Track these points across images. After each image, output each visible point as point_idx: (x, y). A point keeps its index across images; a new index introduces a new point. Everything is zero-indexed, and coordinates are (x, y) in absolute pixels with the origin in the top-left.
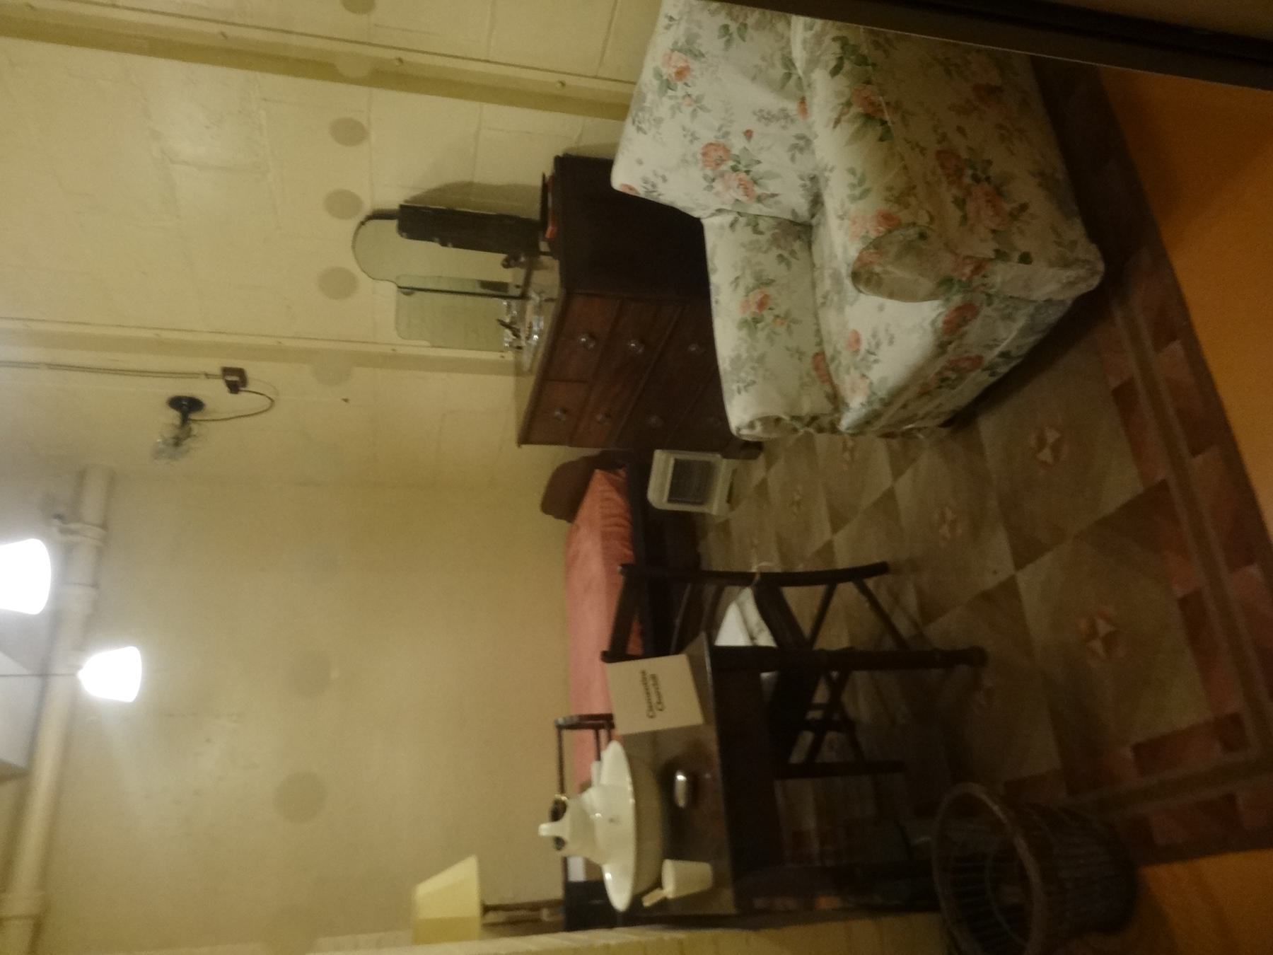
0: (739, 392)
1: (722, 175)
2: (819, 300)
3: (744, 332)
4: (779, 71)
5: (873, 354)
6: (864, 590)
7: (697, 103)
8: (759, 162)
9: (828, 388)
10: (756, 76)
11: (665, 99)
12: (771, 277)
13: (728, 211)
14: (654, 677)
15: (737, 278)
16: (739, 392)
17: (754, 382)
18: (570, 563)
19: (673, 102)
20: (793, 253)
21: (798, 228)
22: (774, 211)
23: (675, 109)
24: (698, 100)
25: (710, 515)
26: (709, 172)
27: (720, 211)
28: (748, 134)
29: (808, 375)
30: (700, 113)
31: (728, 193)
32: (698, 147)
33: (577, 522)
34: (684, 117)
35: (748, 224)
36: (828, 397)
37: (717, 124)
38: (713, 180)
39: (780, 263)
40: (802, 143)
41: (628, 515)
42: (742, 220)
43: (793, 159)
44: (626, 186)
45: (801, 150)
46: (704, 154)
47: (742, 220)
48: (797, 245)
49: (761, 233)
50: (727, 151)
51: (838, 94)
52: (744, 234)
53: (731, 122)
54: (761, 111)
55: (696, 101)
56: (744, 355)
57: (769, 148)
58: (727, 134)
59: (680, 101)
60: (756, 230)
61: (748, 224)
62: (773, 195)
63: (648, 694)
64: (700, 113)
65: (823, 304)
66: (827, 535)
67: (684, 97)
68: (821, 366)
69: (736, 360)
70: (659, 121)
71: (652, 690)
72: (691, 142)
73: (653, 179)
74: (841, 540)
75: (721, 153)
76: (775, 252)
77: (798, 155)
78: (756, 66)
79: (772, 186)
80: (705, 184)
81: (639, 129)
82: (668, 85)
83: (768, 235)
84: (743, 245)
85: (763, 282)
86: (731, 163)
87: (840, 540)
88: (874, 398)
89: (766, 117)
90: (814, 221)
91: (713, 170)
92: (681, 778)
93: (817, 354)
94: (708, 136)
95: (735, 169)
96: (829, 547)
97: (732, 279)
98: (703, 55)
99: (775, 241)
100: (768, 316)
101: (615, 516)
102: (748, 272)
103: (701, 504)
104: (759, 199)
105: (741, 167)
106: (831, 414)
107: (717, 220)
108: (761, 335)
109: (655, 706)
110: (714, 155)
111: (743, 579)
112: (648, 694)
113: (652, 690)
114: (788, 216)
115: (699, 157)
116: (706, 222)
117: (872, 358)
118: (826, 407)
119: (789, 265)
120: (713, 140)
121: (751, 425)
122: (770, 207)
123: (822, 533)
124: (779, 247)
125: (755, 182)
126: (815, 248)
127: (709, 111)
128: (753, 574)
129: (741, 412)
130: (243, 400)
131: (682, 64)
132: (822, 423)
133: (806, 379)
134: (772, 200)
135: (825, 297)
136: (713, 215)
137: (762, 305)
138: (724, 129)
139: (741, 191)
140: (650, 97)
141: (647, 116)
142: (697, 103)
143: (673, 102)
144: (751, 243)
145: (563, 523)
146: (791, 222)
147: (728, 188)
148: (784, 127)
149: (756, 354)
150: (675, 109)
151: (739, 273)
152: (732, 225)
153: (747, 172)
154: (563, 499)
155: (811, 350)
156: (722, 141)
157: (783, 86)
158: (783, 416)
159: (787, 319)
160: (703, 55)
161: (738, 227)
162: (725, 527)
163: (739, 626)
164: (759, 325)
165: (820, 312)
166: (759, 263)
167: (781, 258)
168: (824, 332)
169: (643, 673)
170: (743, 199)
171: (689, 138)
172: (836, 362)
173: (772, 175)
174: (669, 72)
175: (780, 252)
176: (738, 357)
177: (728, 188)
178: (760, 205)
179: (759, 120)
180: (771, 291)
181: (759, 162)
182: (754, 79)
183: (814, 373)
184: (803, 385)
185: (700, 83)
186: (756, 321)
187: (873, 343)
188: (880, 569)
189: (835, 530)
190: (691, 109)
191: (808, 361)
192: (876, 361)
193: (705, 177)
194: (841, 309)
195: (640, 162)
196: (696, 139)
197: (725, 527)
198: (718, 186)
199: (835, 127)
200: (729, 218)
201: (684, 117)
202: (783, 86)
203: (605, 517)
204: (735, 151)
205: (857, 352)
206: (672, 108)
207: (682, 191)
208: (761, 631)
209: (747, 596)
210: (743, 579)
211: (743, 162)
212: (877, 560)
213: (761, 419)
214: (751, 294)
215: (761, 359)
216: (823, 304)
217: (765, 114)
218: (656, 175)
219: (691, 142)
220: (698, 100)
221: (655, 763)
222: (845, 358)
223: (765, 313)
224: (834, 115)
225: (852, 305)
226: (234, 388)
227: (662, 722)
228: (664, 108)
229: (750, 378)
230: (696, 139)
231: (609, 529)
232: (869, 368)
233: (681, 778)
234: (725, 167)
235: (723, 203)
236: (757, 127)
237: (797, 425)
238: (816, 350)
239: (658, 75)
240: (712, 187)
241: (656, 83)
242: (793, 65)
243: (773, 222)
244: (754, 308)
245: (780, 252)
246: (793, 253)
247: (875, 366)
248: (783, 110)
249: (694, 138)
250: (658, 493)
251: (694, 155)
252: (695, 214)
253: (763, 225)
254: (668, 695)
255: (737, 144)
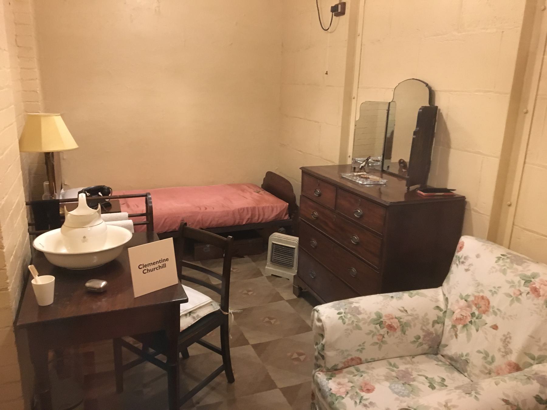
0: (339, 314)
1: (469, 306)
2: (392, 361)
3: (374, 316)
4: (536, 354)
5: (360, 402)
6: (217, 373)
7: (516, 298)
8: (477, 330)
9: (341, 366)
10: (533, 338)
11: (518, 278)
12: (407, 333)
13: (447, 306)
14: (165, 266)
15: (406, 311)
16: (339, 314)
17: (344, 323)
18: (238, 186)
19: (516, 283)
20: (421, 344)
21: (436, 347)
22: (446, 335)
23: (512, 284)
24: (518, 300)
25: (266, 265)
26: (471, 299)
27: (447, 299)
28: (495, 327)
29: (348, 355)
30: (377, 346)
31: (457, 307)
32: (487, 294)
33: (262, 192)
34: (506, 289)
35: (438, 317)
36: (335, 365)
37: (502, 309)
38: (466, 300)
39: (415, 337)
40: (489, 359)
41: (264, 221)
42: (441, 314)
43: (479, 352)
44: (463, 245)
45: (485, 358)
46: (483, 298)
47: (441, 314)
48: (426, 347)
49: (433, 326)
50: (485, 312)
51: (524, 402)
52: (433, 315)
53: (503, 318)
54: (510, 338)
55: (517, 297)
56: (360, 317)
57: (486, 338)
58: (495, 313)
59: (517, 288)
60: (435, 322)
61: (438, 317)
62: (456, 336)
63: (154, 264)
64: (377, 346)
65: (390, 364)
66: (252, 342)
67: (520, 291)
68: (354, 362)
69: (357, 311)
70: (504, 272)
71: (156, 266)
72: (491, 291)
73: (467, 263)
74: (249, 351)
75: (483, 308)
76: (421, 334)
77: (482, 355)
78: (540, 339)
79: (462, 336)
80: (464, 295)
81: (499, 258)
82: (528, 281)
83: (432, 330)
84: (426, 314)
85: (404, 327)
86: (477, 313)
87: (249, 351)
88: (334, 398)
89: (506, 340)
90: (439, 356)
91: (472, 301)
92: (103, 284)
93: (360, 359)
94: (494, 302)
95: (473, 315)
96: (245, 342)
97: (406, 309)
98: (404, 334)
99: (428, 334)
100: (383, 331)
101: (264, 215)
102: (410, 318)
103: (271, 261)
104: (454, 327)
105: (475, 318)
106: (325, 366)
107: (441, 298)
108: (372, 327)
109: (145, 268)
110: (482, 303)
111: (225, 306)
112: (154, 264)
113: (156, 266)
114: (443, 342)
115: (481, 294)
116: (439, 290)
117: (358, 401)
118: (329, 365)
119: (414, 342)
120: (491, 304)
121: (319, 320)
122: (450, 332)
123: (253, 338)
124: (425, 336)
125: (465, 326)
126: (424, 357)
127: (511, 305)
128: (228, 311)
129: (327, 312)
130: (327, 14)
131: (542, 292)
132: (319, 361)
133: (346, 354)
134: (454, 334)
135: (395, 366)
136: (444, 295)
137: (390, 327)
138: (498, 313)
139: (459, 316)
140: (520, 268)
141: (507, 265)
142: (516, 298)
143: (516, 283)
144: (428, 319)
145: (262, 182)
146: (440, 343)
147: (461, 309)
148: (499, 350)
149: (361, 324)
150: (512, 284)
151: (409, 312)
152: (438, 307)
153: (471, 322)
154: (274, 185)
155: (363, 357)
156: (491, 310)
157: (526, 354)
158: (324, 340)
159: (381, 342)
160: (404, 334)
161: (437, 311)
162: (259, 274)
163: (197, 303)
164: (378, 326)
165: (384, 362)
166: (415, 326)
167: (418, 338)
168: (374, 364)
169: (167, 260)
170: (454, 317)
171: (494, 290)
172: (356, 373)
173: (469, 336)
174: (537, 283)
175: (422, 337)
176: (360, 313)
177: (461, 309)
178: (450, 327)
179: (504, 335)
180: (399, 333)
181: (477, 330)
182: (531, 337)
183: (350, 358)
184: (342, 352)
185: (528, 302)
186: (381, 324)
187: (366, 403)
188: (231, 379)
189: (255, 346)
190: (377, 341)
191: (355, 354)
192: (356, 402)
193: (468, 296)
194: (388, 378)
195: (478, 256)
196: (493, 295)
197: (259, 274)
198: (463, 303)
199: (504, 400)
200: (443, 306)
201: (506, 289)
202: (526, 354)
203: (263, 208)
204: (484, 317)
205: (362, 390)
206: (513, 282)
207: (457, 274)
208: (194, 318)
209: (216, 307)
210: (225, 306)
211: (477, 320)
212: (235, 376)
213: (323, 325)
214: (397, 320)
215: (358, 328)
216: (390, 364)
217: (508, 340)
218: (471, 265)
219: (491, 291)
220: (518, 300)
221: (114, 266)
222: (358, 380)
223: (385, 329)
224: (511, 400)
225: (390, 387)
226: (334, 9)
227: (136, 275)
228: (510, 276)
229: (346, 320)
230: (493, 295)
231: (257, 210)
232: (352, 398)
233: (103, 284)
234: (474, 309)
235: (452, 304)
236: (500, 333)
237: (319, 346)
238: (363, 359)
239: (534, 276)
240: (462, 299)
241: (529, 274)
242: (540, 363)
243: (440, 332)
244: (388, 322)
245: (422, 337)
246: (421, 344)
247: (353, 402)
248: (511, 352)
249: (494, 293)
250: (278, 238)
251: (482, 291)
252: (445, 284)
253: (438, 326)
254: (154, 268)
255: (489, 319)
